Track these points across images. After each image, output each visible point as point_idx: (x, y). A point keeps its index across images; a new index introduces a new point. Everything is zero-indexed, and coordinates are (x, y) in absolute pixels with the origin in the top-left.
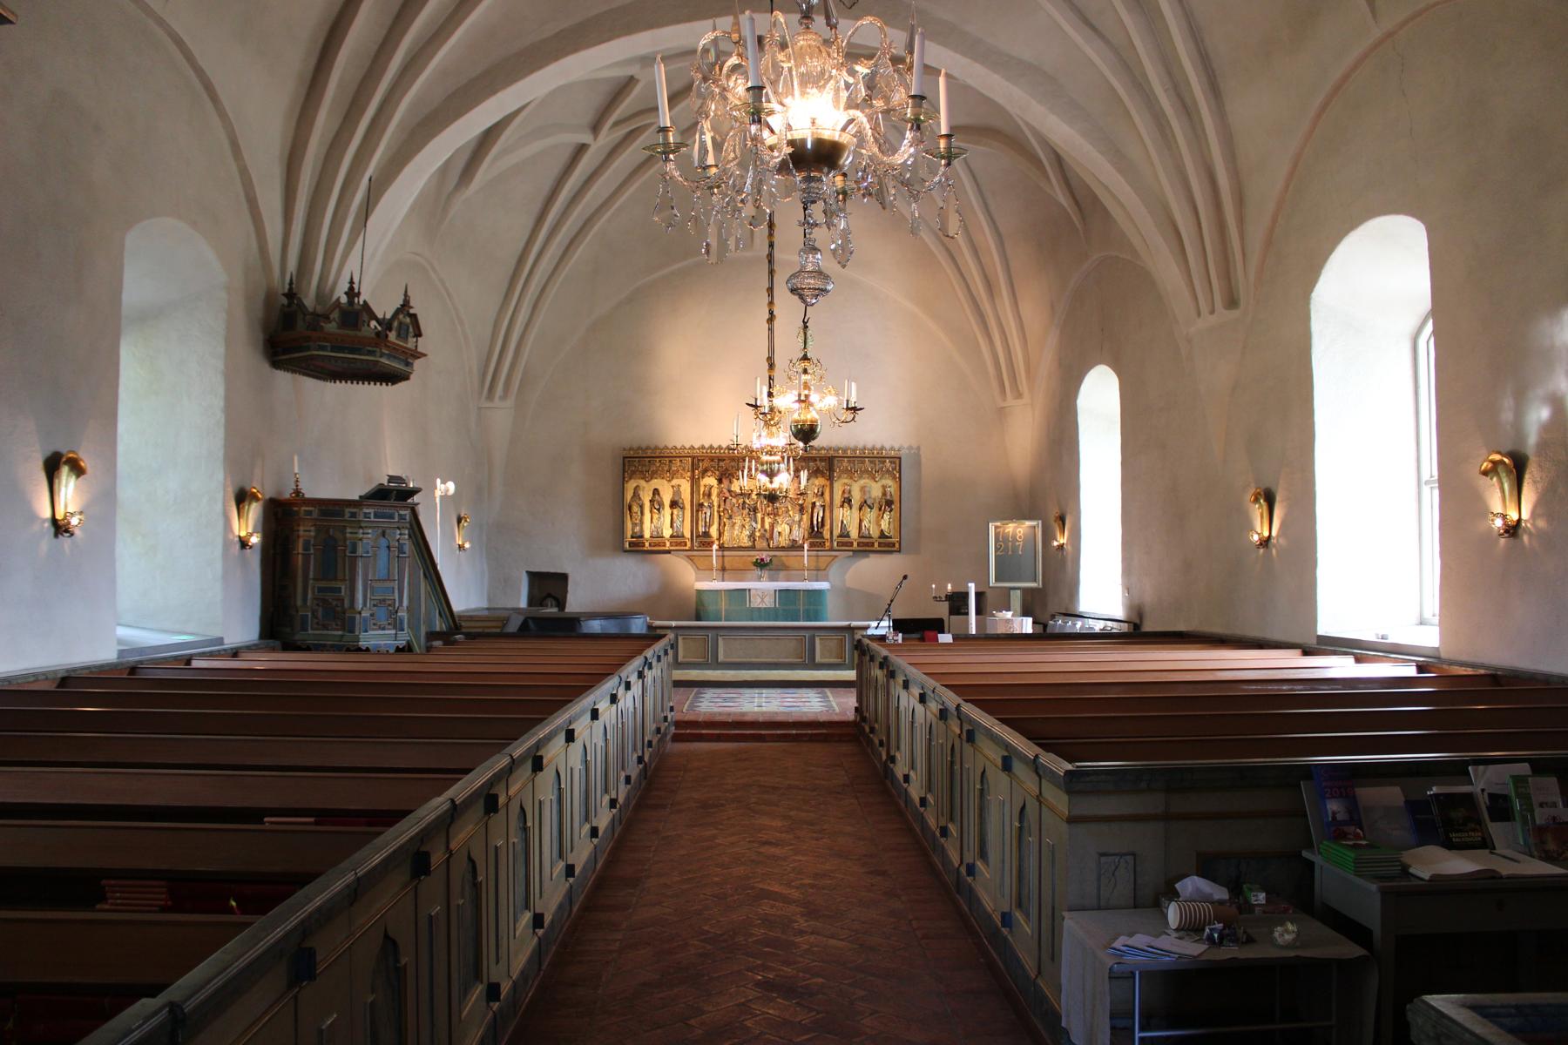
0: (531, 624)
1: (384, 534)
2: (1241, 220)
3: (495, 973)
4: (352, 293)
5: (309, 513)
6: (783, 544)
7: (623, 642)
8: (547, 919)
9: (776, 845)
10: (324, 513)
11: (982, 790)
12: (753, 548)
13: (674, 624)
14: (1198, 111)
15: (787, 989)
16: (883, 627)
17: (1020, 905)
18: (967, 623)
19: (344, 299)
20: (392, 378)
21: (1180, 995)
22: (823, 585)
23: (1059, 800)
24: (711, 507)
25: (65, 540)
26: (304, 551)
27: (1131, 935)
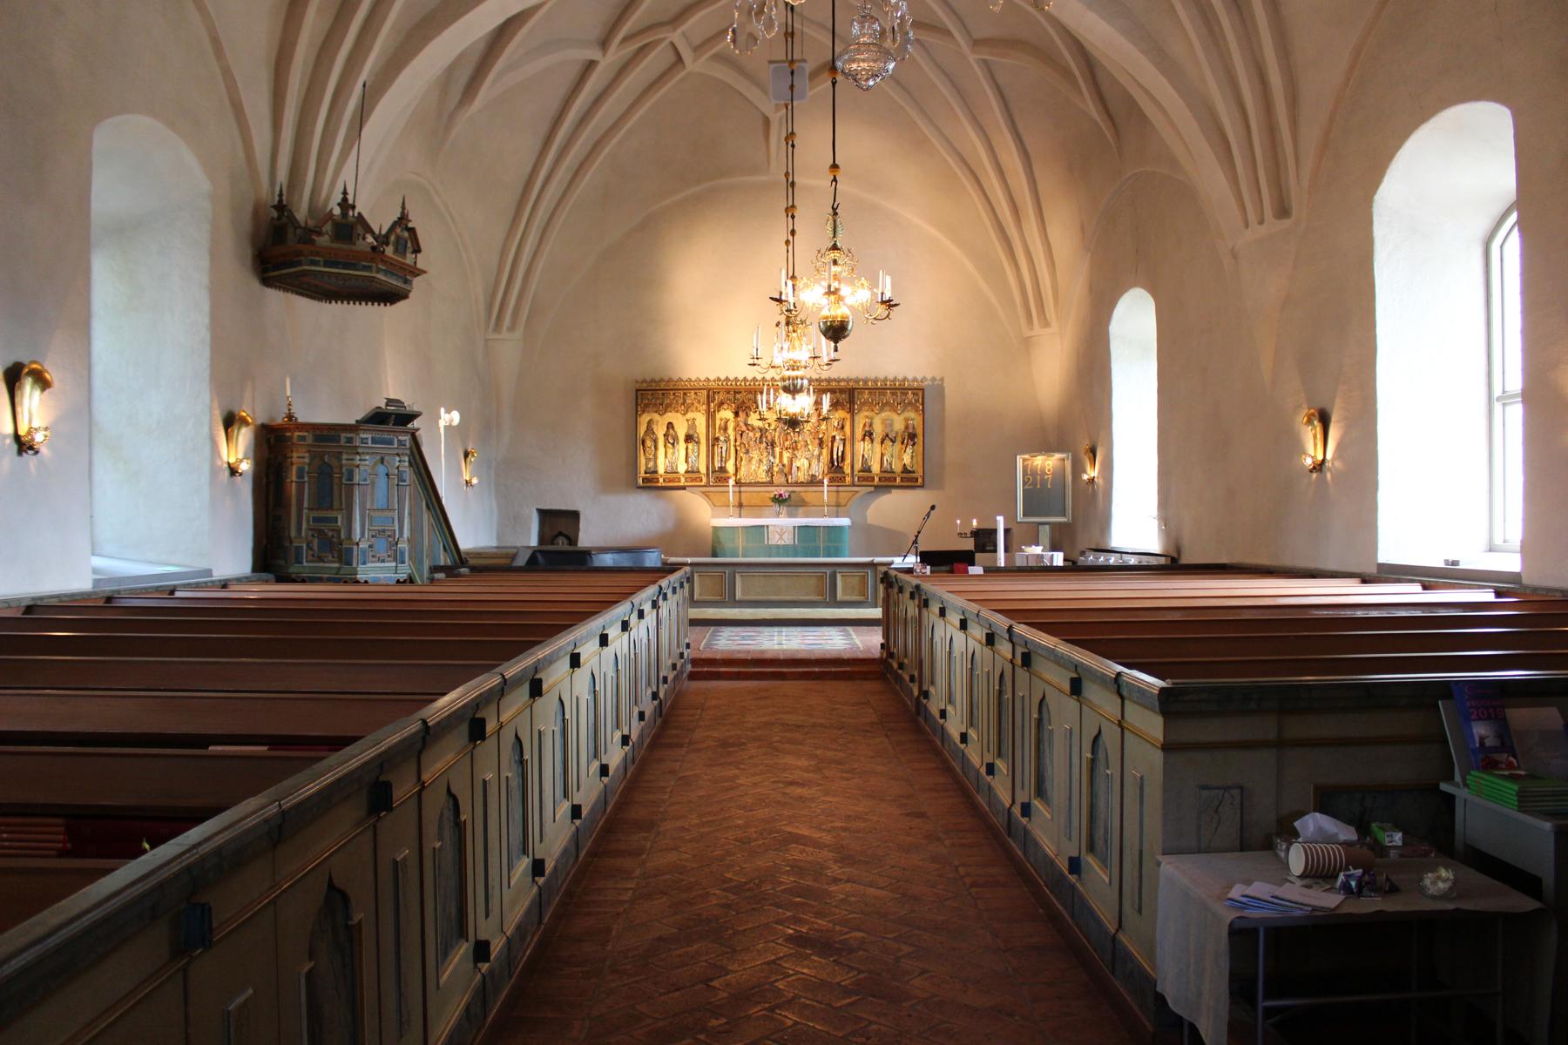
1: (382, 461)
3: (484, 928)
4: (345, 205)
5: (303, 438)
6: (801, 479)
7: (634, 574)
8: (549, 866)
9: (802, 785)
10: (318, 438)
11: (1040, 721)
12: (771, 483)
13: (689, 560)
14: (1224, 38)
15: (823, 945)
16: (912, 560)
17: (1091, 848)
18: (995, 560)
19: (337, 211)
20: (390, 297)
21: (1271, 955)
22: (845, 522)
23: (1153, 725)
24: (727, 441)
25: (28, 457)
26: (297, 482)
27: (1248, 882)
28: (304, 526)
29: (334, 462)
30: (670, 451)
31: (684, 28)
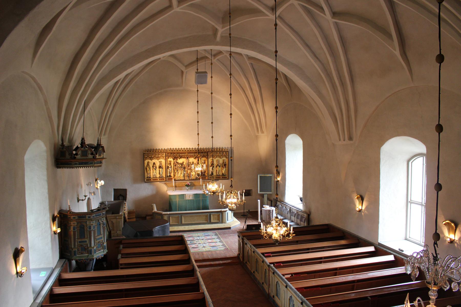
0: (138, 234)
5: (74, 218)
12: (184, 180)
17: (256, 271)
24: (171, 167)
28: (76, 244)
29: (84, 224)
30: (154, 171)
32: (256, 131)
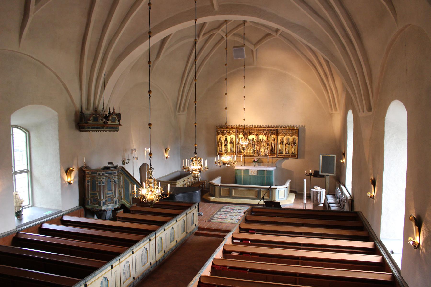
2: (371, 82)
26: (88, 183)
31: (222, 29)
32: (330, 109)
